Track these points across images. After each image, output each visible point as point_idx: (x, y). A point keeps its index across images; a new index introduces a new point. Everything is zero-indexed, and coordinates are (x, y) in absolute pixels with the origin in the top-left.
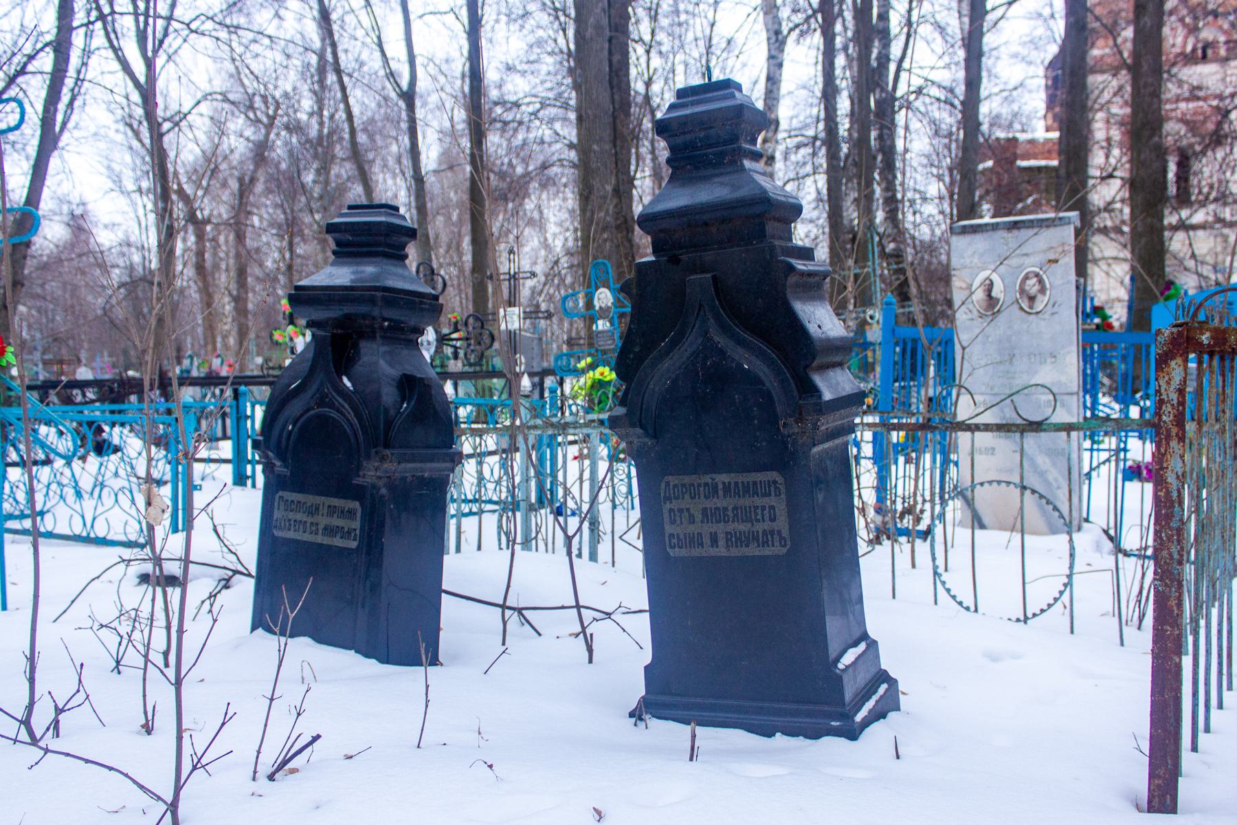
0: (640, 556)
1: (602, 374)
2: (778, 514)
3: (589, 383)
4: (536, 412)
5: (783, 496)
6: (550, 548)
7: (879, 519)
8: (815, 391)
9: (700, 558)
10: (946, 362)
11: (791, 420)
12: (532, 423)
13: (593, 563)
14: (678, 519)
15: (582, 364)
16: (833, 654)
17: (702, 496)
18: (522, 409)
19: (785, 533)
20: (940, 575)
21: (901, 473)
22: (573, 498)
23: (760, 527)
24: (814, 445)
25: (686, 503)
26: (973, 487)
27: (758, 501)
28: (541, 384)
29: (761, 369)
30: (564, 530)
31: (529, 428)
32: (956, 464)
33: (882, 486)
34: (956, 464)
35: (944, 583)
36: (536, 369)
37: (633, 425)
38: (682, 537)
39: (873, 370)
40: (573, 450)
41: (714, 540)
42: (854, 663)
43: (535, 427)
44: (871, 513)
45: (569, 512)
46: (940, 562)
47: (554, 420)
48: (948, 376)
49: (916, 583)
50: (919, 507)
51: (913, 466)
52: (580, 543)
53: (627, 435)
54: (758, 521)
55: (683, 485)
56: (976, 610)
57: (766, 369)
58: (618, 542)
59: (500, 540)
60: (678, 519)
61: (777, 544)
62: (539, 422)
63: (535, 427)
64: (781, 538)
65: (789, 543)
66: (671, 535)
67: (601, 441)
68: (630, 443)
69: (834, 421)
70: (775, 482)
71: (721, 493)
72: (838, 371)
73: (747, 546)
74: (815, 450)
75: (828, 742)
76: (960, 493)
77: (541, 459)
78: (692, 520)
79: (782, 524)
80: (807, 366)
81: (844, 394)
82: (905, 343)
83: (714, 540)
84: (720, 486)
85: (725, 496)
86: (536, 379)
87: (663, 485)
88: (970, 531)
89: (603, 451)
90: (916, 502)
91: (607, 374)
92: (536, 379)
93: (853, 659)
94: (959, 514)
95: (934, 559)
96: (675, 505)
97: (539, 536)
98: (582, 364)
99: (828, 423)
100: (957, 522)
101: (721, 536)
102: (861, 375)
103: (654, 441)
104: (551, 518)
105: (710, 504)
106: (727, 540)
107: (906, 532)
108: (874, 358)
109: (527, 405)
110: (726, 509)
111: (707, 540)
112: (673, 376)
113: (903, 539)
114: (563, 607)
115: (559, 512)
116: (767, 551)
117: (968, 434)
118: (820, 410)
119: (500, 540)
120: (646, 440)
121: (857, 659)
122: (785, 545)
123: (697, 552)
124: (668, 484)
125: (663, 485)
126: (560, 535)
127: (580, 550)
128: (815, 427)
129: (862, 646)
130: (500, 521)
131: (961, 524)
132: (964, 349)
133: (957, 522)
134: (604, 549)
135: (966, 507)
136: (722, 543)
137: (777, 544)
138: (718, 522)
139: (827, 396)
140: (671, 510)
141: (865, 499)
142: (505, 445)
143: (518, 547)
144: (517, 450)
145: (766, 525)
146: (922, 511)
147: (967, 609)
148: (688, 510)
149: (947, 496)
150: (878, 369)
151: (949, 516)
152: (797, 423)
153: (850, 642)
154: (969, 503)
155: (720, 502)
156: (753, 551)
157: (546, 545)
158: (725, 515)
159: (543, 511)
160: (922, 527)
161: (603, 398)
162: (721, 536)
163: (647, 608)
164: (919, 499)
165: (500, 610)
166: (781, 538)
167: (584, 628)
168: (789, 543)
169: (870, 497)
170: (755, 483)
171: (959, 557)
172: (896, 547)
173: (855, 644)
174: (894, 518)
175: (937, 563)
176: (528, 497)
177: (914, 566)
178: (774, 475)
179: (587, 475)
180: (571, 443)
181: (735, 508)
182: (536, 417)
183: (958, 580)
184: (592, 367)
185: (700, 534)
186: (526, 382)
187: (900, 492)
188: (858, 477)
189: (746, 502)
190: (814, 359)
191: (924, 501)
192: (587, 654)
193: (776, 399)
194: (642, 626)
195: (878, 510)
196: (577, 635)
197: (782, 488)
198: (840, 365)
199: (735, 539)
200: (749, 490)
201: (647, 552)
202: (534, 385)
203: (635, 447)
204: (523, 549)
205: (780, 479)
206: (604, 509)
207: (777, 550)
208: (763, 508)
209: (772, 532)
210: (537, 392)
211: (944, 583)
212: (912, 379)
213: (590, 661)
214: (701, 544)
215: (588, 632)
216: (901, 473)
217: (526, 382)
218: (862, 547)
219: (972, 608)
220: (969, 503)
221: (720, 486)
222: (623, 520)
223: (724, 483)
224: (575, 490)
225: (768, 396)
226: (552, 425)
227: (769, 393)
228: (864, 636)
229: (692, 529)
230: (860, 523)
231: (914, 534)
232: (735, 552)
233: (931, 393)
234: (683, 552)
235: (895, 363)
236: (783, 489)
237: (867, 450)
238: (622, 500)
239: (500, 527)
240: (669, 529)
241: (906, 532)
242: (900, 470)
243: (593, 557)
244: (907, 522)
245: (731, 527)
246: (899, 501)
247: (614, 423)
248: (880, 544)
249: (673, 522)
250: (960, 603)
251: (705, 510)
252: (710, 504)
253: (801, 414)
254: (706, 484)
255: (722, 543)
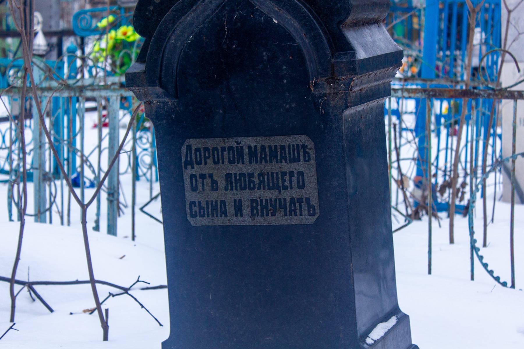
0: (161, 226)
1: (125, 34)
2: (306, 180)
3: (111, 43)
4: (52, 73)
5: (313, 162)
6: (65, 219)
7: (419, 193)
8: (349, 49)
9: (225, 229)
10: (492, 27)
11: (322, 80)
12: (45, 85)
13: (111, 237)
14: (200, 186)
15: (104, 23)
16: (361, 328)
17: (226, 161)
18: (35, 69)
19: (314, 201)
20: (477, 250)
21: (443, 145)
22: (91, 166)
23: (287, 195)
24: (347, 107)
25: (208, 168)
26: (514, 157)
27: (287, 167)
28: (60, 45)
29: (293, 25)
30: (81, 202)
31: (43, 90)
32: (500, 137)
33: (423, 159)
34: (500, 137)
35: (481, 258)
36: (54, 29)
37: (151, 83)
38: (204, 205)
39: (419, 37)
40: (91, 119)
41: (238, 209)
42: (383, 338)
43: (49, 89)
44: (411, 186)
45: (88, 184)
46: (479, 236)
47: (71, 82)
48: (495, 45)
49: (453, 257)
50: (460, 180)
51: (455, 139)
52: (98, 214)
53: (146, 94)
54: (285, 188)
55: (206, 149)
56: (513, 286)
57: (296, 24)
58: (139, 214)
59: (10, 211)
60: (200, 186)
61: (305, 213)
62: (54, 84)
63: (49, 89)
64: (310, 206)
65: (318, 211)
66: (193, 203)
67: (122, 107)
68: (149, 103)
69: (368, 82)
70: (304, 147)
71: (246, 157)
72: (374, 28)
73: (273, 215)
74: (348, 112)
75: (109, 324)
76: (499, 163)
77: (56, 125)
78: (215, 186)
79: (311, 191)
80: (341, 22)
81: (379, 53)
82: (451, 7)
83: (238, 209)
84: (246, 151)
85: (250, 162)
86: (54, 40)
87: (184, 149)
88: (509, 206)
89: (125, 118)
90: (457, 176)
91: (129, 33)
92: (54, 40)
93: (382, 334)
94: (500, 189)
95: (472, 233)
96: (197, 170)
97: (54, 207)
98: (104, 23)
99: (362, 83)
100: (498, 196)
101: (246, 204)
102: (405, 41)
103: (175, 101)
104: (66, 189)
105: (235, 169)
106: (252, 209)
107: (446, 207)
108: (420, 25)
109: (42, 65)
110: (251, 175)
111: (230, 209)
112: (197, 30)
113: (443, 215)
114: (77, 282)
115: (76, 183)
116: (295, 221)
117: (511, 102)
118: (354, 70)
119: (10, 211)
120: (166, 99)
121: (386, 334)
122: (314, 214)
123: (219, 221)
124: (189, 147)
125: (184, 149)
126: (76, 208)
127: (97, 222)
128: (348, 87)
129: (393, 321)
130: (11, 190)
131: (502, 198)
132: (509, 12)
133: (498, 196)
134: (123, 222)
135: (508, 181)
136: (246, 211)
137: (305, 213)
138: (243, 189)
139: (362, 55)
140: (192, 176)
141: (404, 171)
142: (16, 112)
143: (29, 220)
144: (29, 116)
145: (295, 193)
146: (464, 185)
147: (504, 284)
148: (211, 176)
149: (488, 169)
150: (423, 35)
151: (490, 191)
152: (329, 83)
153: (381, 315)
154: (510, 174)
155: (244, 168)
156: (279, 220)
157: (62, 218)
158: (250, 182)
159: (58, 183)
160: (465, 203)
161: (126, 60)
162: (246, 204)
163: (165, 283)
164: (461, 173)
165: (8, 284)
166: (310, 206)
167: (99, 305)
168: (318, 211)
169: (410, 169)
170: (283, 147)
171: (498, 232)
172: (435, 223)
173: (385, 319)
174: (434, 191)
175: (475, 237)
176: (42, 165)
177: (452, 241)
178: (303, 139)
179: (105, 143)
180: (89, 110)
181: (261, 175)
182: (50, 78)
183: (496, 256)
184: (115, 26)
185: (223, 202)
186: (40, 42)
187: (441, 164)
188: (397, 149)
189: (273, 167)
190: (348, 14)
191: (466, 174)
192: (101, 331)
193: (307, 57)
194: (160, 303)
195: (418, 184)
196: (92, 312)
197: (312, 153)
198: (376, 22)
199: (259, 208)
200: (275, 155)
201: (167, 224)
202: (50, 46)
203: (154, 107)
204: (36, 221)
205: (310, 144)
206: (126, 180)
207: (306, 219)
208: (292, 174)
209: (300, 201)
210: (55, 53)
211: (481, 258)
212: (459, 48)
213: (106, 338)
214: (224, 213)
215: (103, 307)
216: (443, 145)
217: (40, 42)
218: (397, 220)
219: (509, 284)
220: (510, 174)
221: (246, 151)
222: (144, 192)
223: (250, 147)
224: (93, 160)
225: (298, 52)
226: (68, 87)
227: (300, 50)
228: (395, 310)
229: (214, 196)
230: (396, 195)
231: (453, 209)
232: (260, 221)
233: (475, 62)
234: (205, 222)
235: (440, 31)
236: (313, 155)
237: (409, 121)
238: (145, 170)
239: (11, 197)
240: (190, 196)
241: (446, 207)
242: (440, 144)
243: (112, 230)
244: (446, 197)
245: (257, 194)
246: (440, 173)
247: (132, 81)
248: (419, 219)
249: (194, 189)
250: (497, 279)
251: (228, 176)
252: (235, 169)
253: (333, 74)
254: (231, 148)
255: (246, 211)
